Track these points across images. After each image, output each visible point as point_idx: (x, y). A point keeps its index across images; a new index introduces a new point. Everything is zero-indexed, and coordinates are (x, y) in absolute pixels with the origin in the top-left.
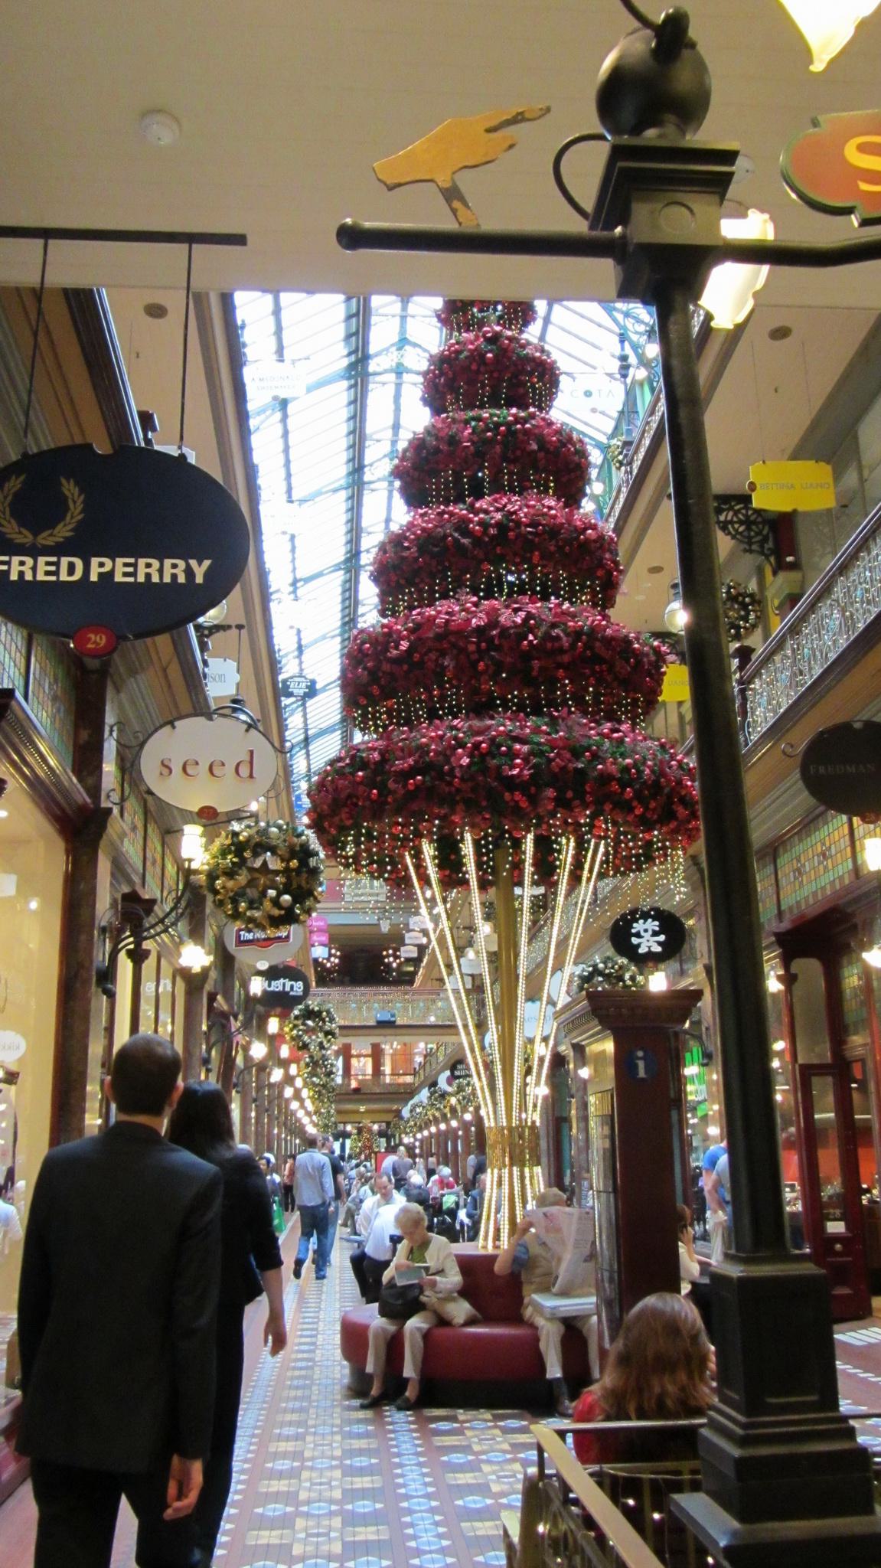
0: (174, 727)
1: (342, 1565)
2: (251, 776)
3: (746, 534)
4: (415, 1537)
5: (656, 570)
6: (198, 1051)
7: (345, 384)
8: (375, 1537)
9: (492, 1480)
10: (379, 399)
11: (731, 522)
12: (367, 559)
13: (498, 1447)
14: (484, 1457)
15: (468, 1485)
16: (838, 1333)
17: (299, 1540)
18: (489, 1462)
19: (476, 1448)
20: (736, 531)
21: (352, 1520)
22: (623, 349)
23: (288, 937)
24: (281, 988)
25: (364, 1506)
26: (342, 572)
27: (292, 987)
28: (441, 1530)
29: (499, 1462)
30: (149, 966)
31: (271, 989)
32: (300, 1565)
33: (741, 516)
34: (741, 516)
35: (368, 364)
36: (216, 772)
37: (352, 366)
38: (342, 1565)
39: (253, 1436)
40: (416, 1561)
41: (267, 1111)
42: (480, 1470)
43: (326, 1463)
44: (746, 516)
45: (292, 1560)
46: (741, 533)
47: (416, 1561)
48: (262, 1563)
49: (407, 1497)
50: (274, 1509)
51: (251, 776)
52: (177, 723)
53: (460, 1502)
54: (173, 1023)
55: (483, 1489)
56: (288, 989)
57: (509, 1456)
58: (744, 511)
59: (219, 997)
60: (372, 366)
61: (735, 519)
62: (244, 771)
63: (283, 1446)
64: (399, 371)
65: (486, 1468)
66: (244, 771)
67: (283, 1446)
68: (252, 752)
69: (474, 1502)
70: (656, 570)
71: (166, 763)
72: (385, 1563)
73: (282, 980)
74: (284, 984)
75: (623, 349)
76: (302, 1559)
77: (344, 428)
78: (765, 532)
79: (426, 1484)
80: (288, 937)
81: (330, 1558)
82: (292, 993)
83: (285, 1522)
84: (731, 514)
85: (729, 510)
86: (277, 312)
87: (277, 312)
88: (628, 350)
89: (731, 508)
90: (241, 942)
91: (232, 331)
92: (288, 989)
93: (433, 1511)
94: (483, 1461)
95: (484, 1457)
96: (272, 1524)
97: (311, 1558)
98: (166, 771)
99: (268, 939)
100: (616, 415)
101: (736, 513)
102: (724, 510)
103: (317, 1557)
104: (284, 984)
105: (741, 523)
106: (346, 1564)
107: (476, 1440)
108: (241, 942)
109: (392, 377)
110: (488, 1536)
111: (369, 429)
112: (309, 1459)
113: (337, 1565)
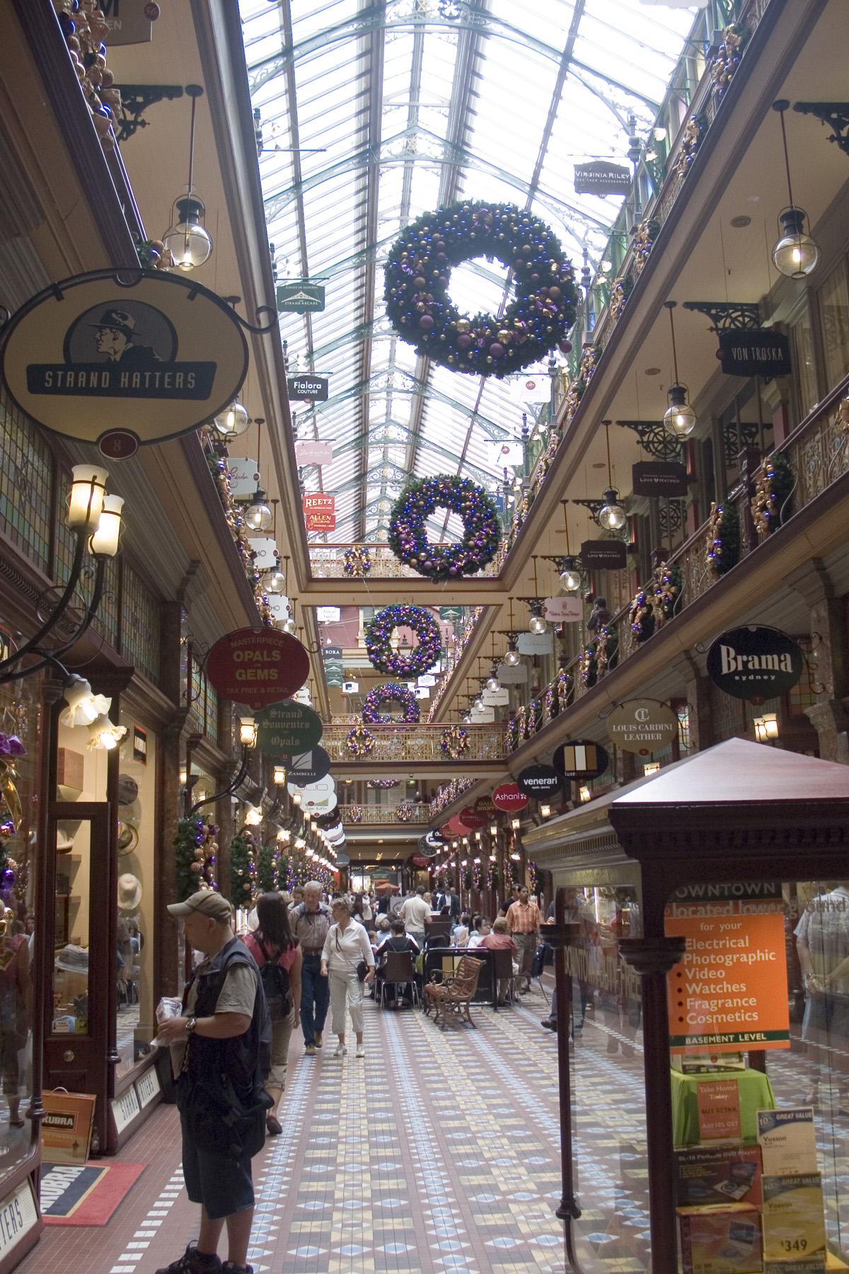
3: (663, 451)
4: (435, 1227)
5: (653, 372)
7: (353, 274)
8: (401, 1227)
9: (500, 1182)
10: (390, 185)
11: (653, 442)
12: (383, 253)
13: (523, 1186)
14: (511, 1197)
15: (513, 1261)
17: (337, 1230)
18: (515, 1202)
19: (503, 1188)
20: (656, 449)
21: (380, 1213)
22: (586, 264)
25: (388, 1167)
28: (457, 1221)
29: (551, 1248)
35: (375, 253)
37: (358, 329)
39: (292, 1145)
43: (357, 1168)
46: (659, 451)
49: (437, 1239)
50: (319, 1169)
53: (490, 1243)
55: (511, 1230)
57: (535, 1196)
58: (741, 319)
60: (384, 153)
61: (655, 440)
63: (319, 1154)
64: (389, 389)
67: (319, 1154)
69: (486, 1198)
70: (653, 372)
75: (586, 264)
77: (355, 88)
78: (677, 450)
79: (444, 1186)
83: (325, 1215)
84: (729, 320)
85: (650, 432)
86: (308, 325)
87: (308, 325)
88: (589, 265)
89: (729, 316)
91: (247, 117)
93: (463, 1252)
94: (479, 1138)
95: (511, 1197)
96: (311, 1216)
100: (620, 205)
102: (722, 317)
103: (352, 1258)
105: (660, 442)
109: (384, 395)
110: (513, 1262)
111: (381, 207)
112: (341, 1164)
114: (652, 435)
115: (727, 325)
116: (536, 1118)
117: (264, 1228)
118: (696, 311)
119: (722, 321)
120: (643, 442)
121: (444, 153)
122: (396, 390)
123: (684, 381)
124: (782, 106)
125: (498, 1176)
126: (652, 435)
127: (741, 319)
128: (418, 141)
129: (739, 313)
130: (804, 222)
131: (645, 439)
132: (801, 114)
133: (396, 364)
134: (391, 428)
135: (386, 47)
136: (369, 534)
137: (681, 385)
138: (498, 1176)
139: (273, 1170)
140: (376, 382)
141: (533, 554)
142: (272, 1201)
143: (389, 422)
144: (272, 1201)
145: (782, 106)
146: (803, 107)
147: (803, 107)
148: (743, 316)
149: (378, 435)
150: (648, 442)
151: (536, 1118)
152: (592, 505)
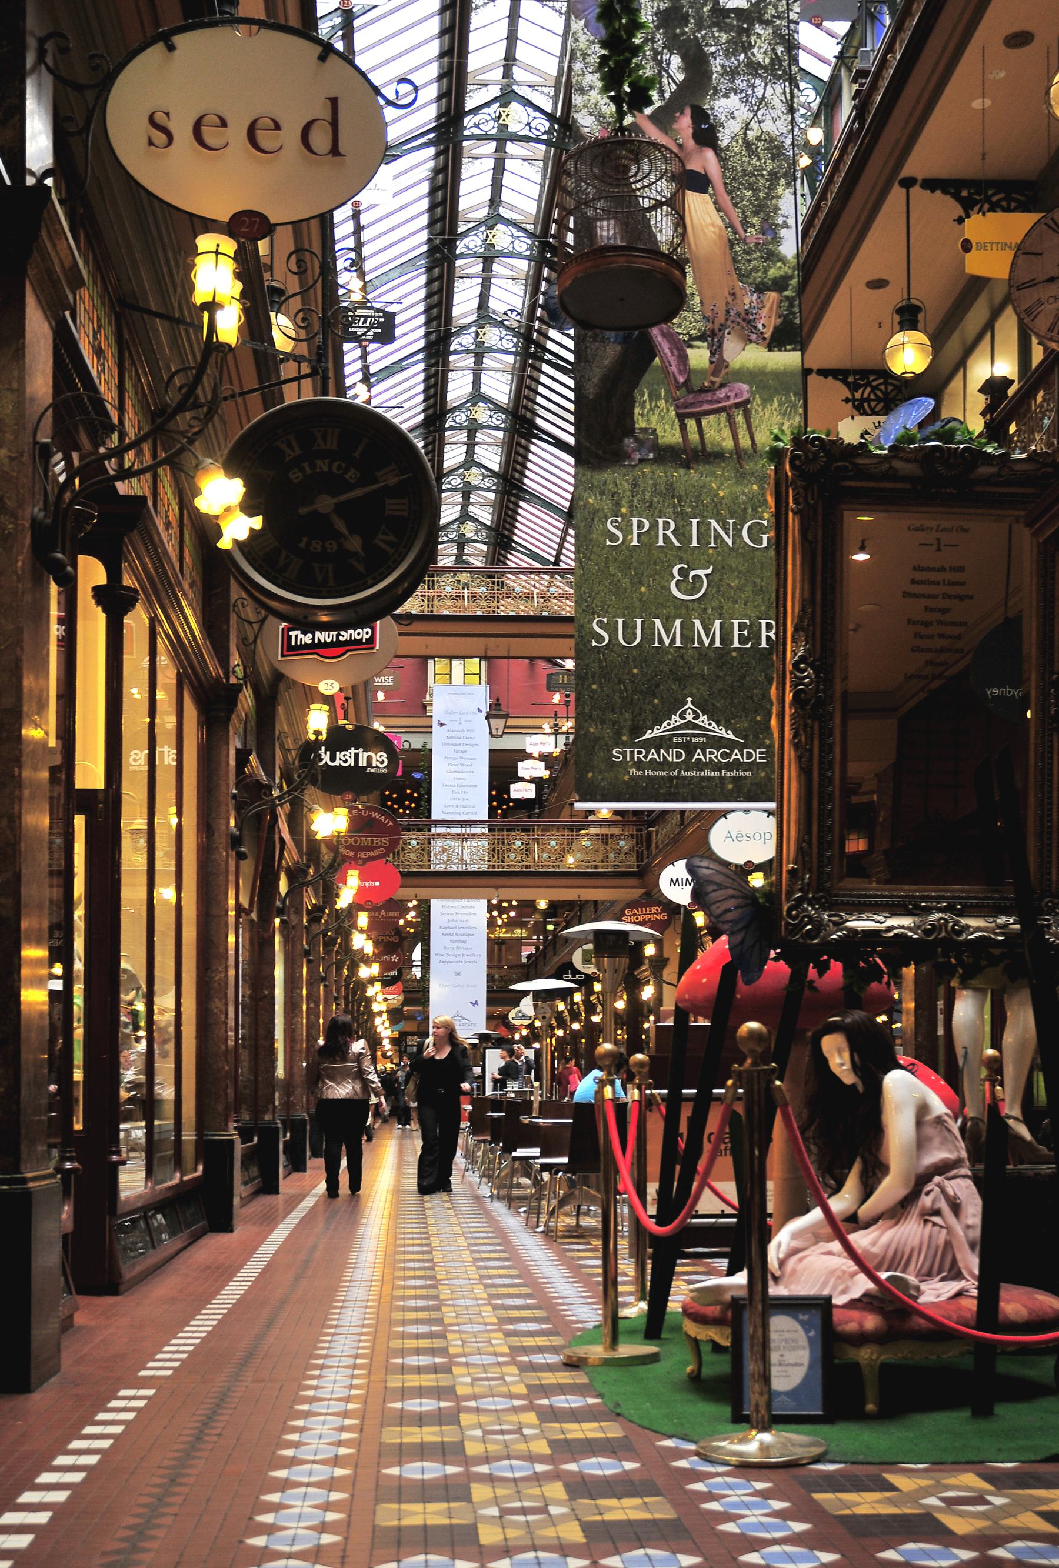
0: (171, 48)
1: (595, 1563)
2: (335, 151)
5: (878, 284)
6: (223, 822)
11: (868, 400)
16: (1008, 1301)
23: (371, 640)
24: (351, 762)
26: (431, 151)
27: (369, 758)
30: (136, 621)
31: (337, 763)
32: (506, 1562)
33: (878, 393)
34: (878, 393)
36: (264, 143)
38: (595, 1563)
40: (753, 1558)
41: (323, 979)
42: (552, 1443)
44: (885, 393)
45: (484, 1554)
47: (753, 1558)
48: (421, 1558)
51: (335, 151)
52: (177, 39)
54: (179, 814)
56: (362, 763)
59: (253, 759)
61: (872, 396)
62: (320, 140)
65: (542, 1447)
66: (320, 140)
68: (334, 102)
70: (878, 284)
71: (160, 118)
72: (687, 1560)
73: (353, 751)
74: (357, 756)
76: (506, 1551)
80: (371, 640)
81: (565, 1550)
82: (369, 770)
85: (865, 386)
89: (869, 384)
90: (292, 649)
92: (362, 763)
97: (523, 1549)
98: (160, 138)
99: (338, 643)
101: (874, 389)
102: (860, 386)
104: (357, 756)
106: (605, 1562)
107: (478, 1433)
108: (292, 649)
111: (474, 62)
113: (586, 1563)
114: (869, 389)
115: (866, 395)
116: (711, 1497)
117: (290, 1518)
118: (938, 192)
119: (860, 391)
120: (854, 400)
121: (530, 249)
122: (516, 138)
123: (920, 294)
124: (908, 183)
125: (534, 1437)
126: (869, 389)
127: (882, 387)
128: (498, 234)
129: (881, 381)
130: (921, 316)
131: (858, 395)
132: (822, 378)
133: (502, 211)
134: (515, 107)
135: (471, 35)
136: (453, 410)
137: (914, 302)
138: (534, 1437)
139: (298, 1474)
140: (476, 119)
141: (905, 173)
142: (300, 1485)
143: (493, 219)
144: (300, 1485)
145: (908, 183)
146: (931, 184)
147: (931, 184)
148: (886, 383)
149: (472, 243)
150: (862, 400)
151: (711, 1497)
152: (851, 379)
